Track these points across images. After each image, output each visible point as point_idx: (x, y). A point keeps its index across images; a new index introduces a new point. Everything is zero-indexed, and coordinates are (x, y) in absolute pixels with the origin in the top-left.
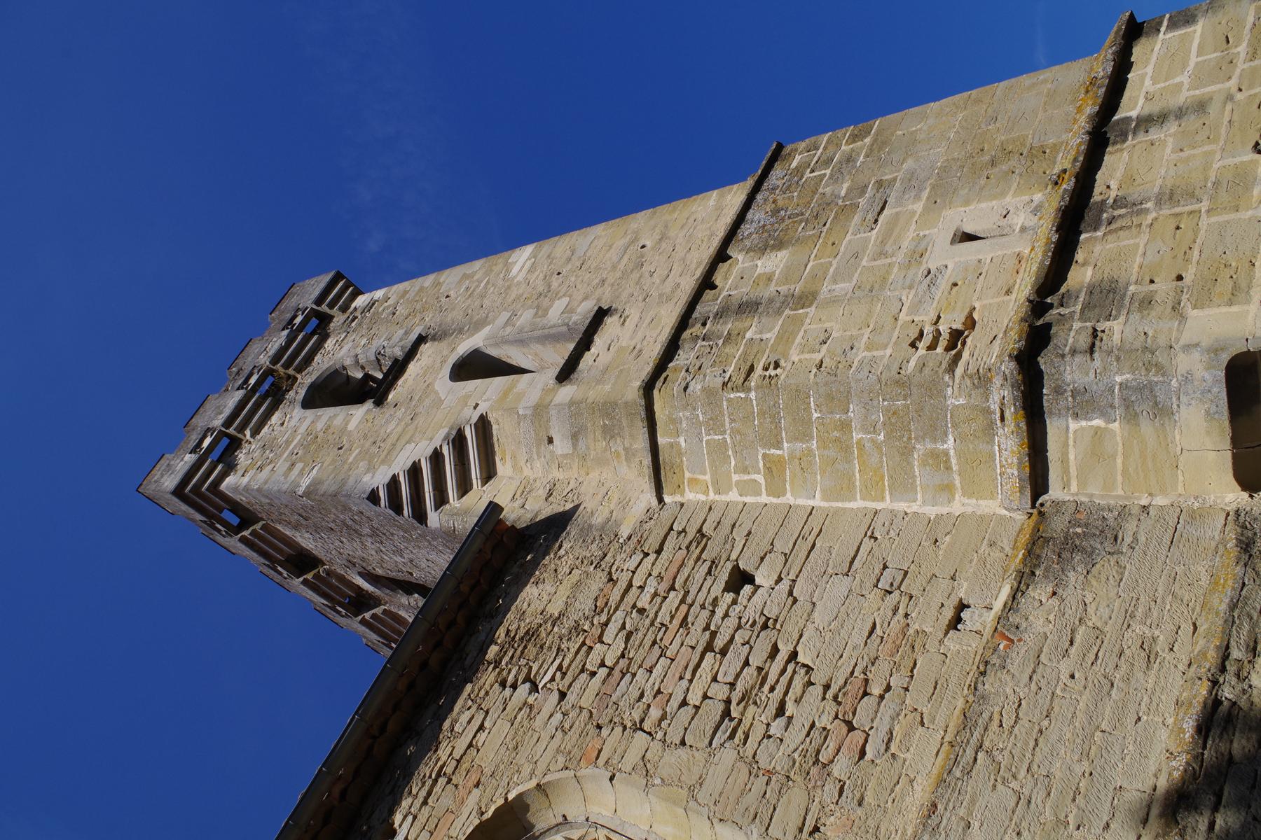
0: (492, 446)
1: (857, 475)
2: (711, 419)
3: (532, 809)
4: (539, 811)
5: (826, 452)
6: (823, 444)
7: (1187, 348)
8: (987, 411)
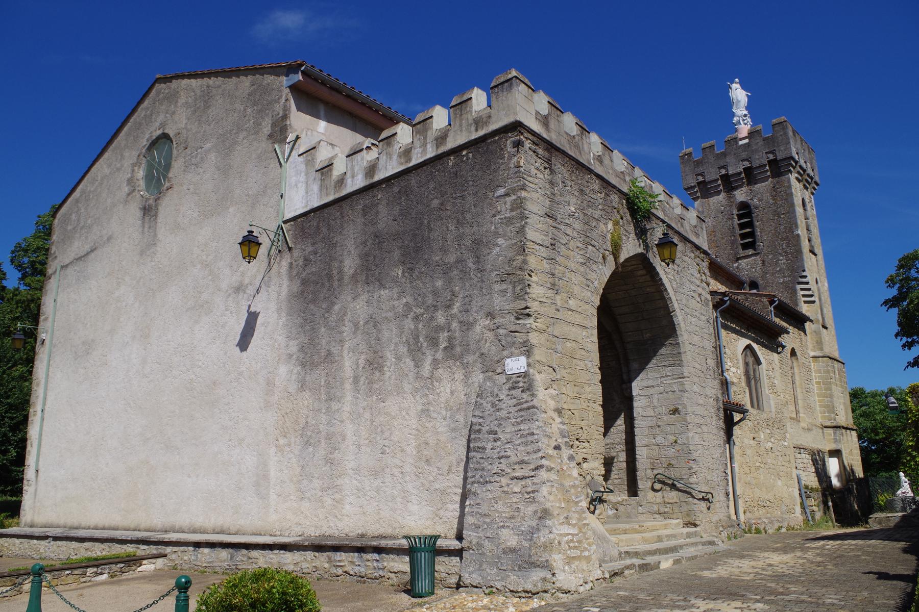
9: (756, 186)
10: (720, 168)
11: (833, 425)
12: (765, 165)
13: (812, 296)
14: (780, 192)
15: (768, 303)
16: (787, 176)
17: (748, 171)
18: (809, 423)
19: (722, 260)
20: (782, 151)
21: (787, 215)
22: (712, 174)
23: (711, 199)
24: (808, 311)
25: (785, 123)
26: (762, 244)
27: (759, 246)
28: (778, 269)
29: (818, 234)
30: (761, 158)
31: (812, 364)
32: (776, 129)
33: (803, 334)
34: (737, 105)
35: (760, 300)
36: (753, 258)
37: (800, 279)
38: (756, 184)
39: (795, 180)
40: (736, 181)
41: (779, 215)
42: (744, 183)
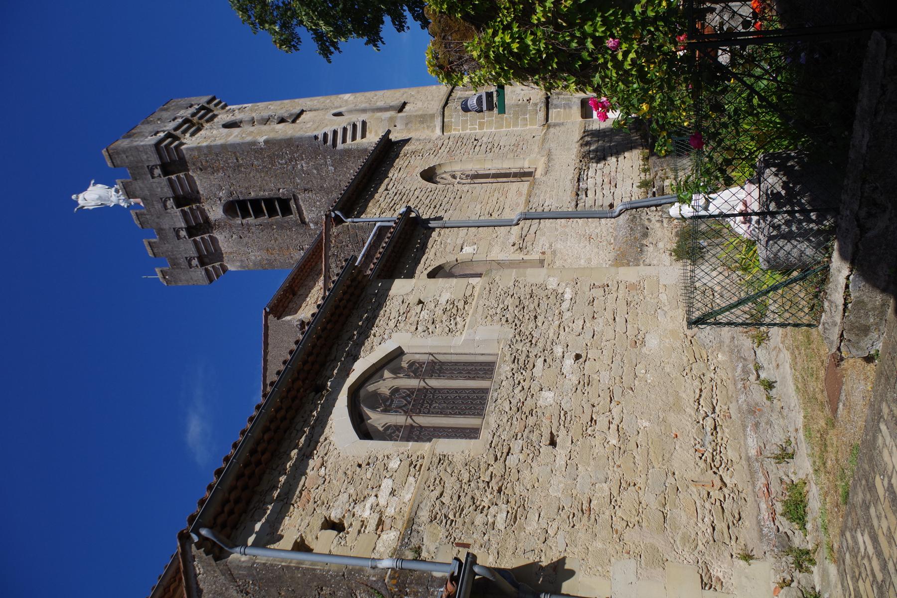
9: (201, 192)
10: (179, 237)
11: (543, 109)
12: (170, 180)
13: (355, 126)
14: (207, 162)
15: (340, 226)
16: (184, 152)
17: (180, 202)
18: (539, 152)
19: (306, 243)
20: (148, 157)
21: (238, 155)
22: (187, 248)
23: (223, 249)
24: (376, 132)
25: (111, 152)
26: (281, 191)
27: (283, 193)
28: (315, 172)
29: (279, 102)
30: (160, 185)
31: (453, 132)
32: (119, 162)
33: (406, 148)
34: (105, 200)
35: (335, 237)
36: (301, 203)
37: (328, 144)
38: (198, 192)
39: (194, 138)
40: (195, 218)
41: (240, 166)
42: (198, 207)
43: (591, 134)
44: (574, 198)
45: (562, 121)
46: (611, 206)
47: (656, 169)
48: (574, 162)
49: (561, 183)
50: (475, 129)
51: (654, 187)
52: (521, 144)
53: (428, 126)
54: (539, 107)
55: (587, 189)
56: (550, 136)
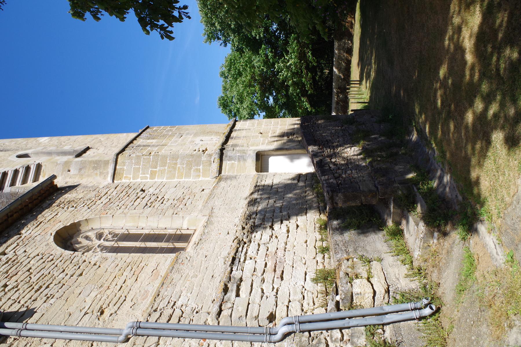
0: (40, 173)
1: (177, 174)
2: (137, 162)
3: (82, 226)
4: (84, 226)
5: (169, 169)
6: (169, 167)
7: (250, 150)
8: (210, 161)
11: (217, 160)
31: (124, 181)
43: (263, 190)
44: (220, 295)
45: (235, 174)
46: (272, 318)
47: (339, 256)
48: (235, 228)
49: (211, 263)
50: (146, 178)
51: (337, 294)
52: (186, 198)
53: (100, 173)
54: (213, 158)
55: (241, 280)
56: (219, 190)
